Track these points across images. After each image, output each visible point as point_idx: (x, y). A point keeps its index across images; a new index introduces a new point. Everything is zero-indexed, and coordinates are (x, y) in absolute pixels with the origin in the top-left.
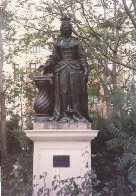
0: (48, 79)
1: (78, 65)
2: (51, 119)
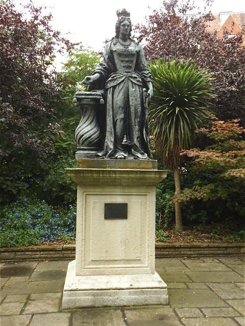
0: (99, 97)
1: (140, 80)
2: (100, 154)
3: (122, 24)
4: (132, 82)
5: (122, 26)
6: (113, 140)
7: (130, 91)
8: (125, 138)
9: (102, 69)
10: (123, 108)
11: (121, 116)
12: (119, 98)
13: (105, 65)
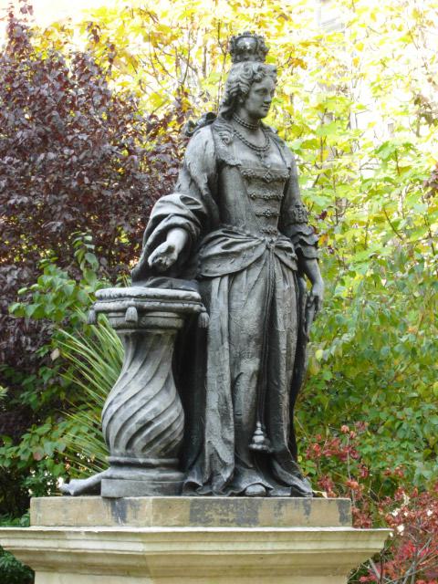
3: (258, 86)
4: (282, 262)
5: (257, 91)
6: (231, 437)
7: (278, 290)
8: (259, 431)
9: (192, 215)
10: (258, 341)
11: (250, 365)
12: (250, 312)
13: (196, 203)
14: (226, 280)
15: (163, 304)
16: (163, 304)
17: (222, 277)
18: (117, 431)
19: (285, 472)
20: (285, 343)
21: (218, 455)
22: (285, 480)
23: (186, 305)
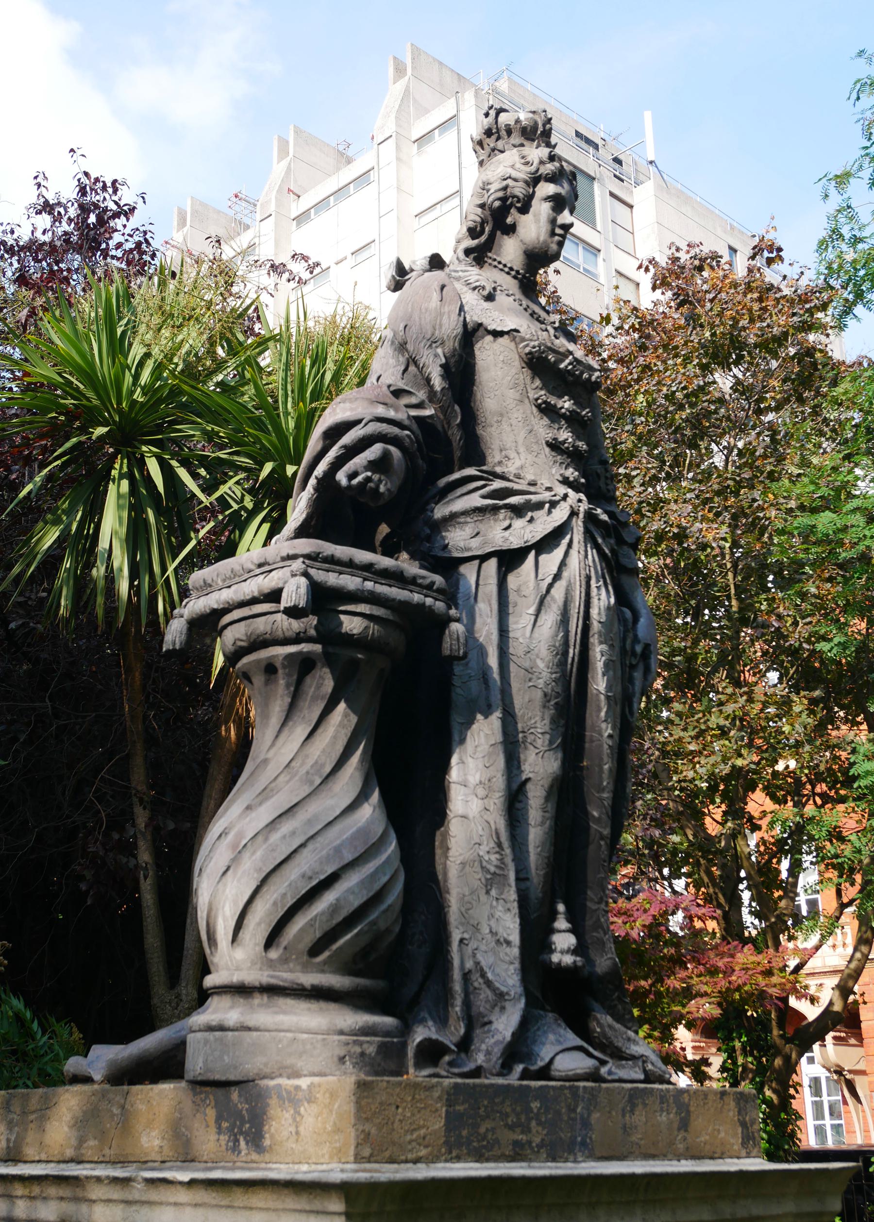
8: (562, 923)
14: (492, 565)
15: (369, 585)
16: (369, 585)
17: (483, 558)
18: (232, 924)
19: (618, 1026)
20: (602, 727)
21: (483, 975)
22: (619, 1043)
23: (417, 597)
